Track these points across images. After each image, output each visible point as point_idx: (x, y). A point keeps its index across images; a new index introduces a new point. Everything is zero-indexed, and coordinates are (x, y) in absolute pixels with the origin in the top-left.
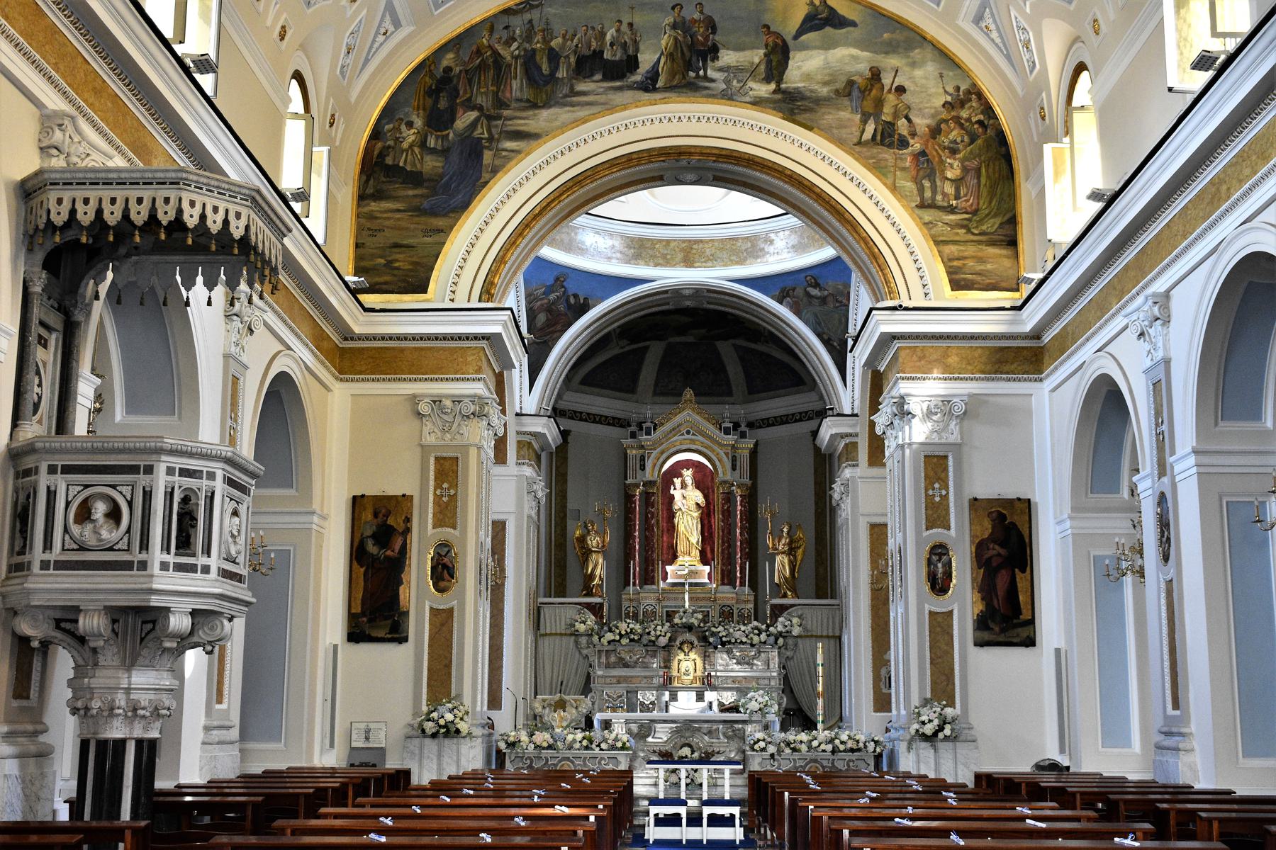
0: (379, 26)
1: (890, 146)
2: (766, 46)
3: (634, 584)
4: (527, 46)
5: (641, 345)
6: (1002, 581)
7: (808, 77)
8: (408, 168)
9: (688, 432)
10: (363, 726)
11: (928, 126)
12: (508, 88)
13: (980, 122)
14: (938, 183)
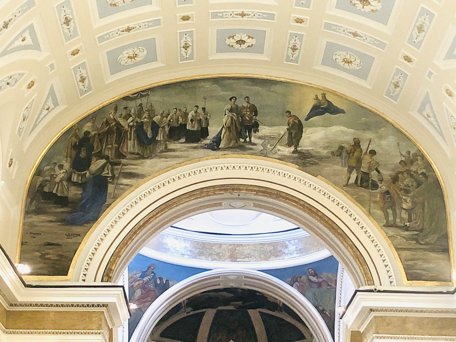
1: (366, 187)
4: (139, 120)
7: (314, 143)
12: (126, 144)
13: (422, 174)
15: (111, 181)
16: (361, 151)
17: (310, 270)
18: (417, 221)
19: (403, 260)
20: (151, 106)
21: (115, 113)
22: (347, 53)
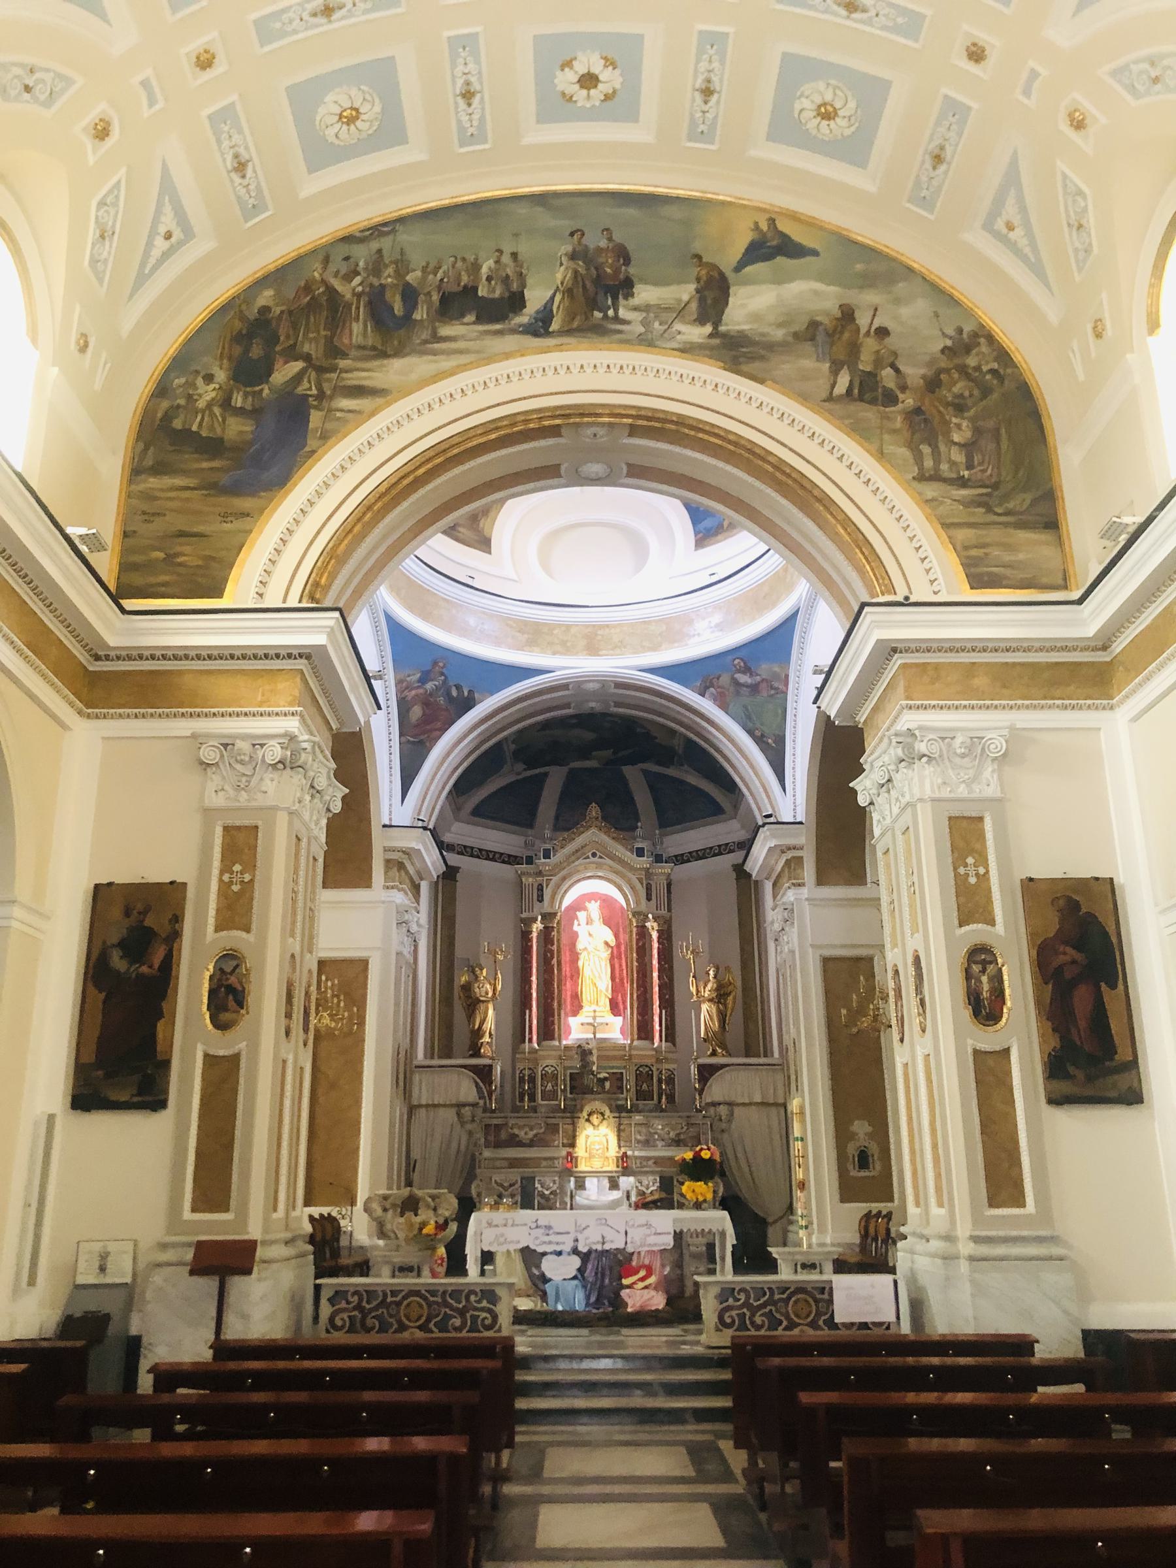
0: (156, 221)
1: (873, 402)
2: (698, 280)
3: (530, 1040)
4: (376, 282)
5: (537, 771)
6: (1081, 998)
7: (756, 317)
8: (204, 434)
9: (594, 855)
10: (97, 1247)
11: (924, 377)
12: (347, 331)
13: (993, 372)
14: (942, 448)
15: (315, 403)
16: (858, 330)
17: (736, 662)
18: (985, 467)
19: (959, 548)
20: (402, 253)
21: (325, 268)
22: (828, 84)
